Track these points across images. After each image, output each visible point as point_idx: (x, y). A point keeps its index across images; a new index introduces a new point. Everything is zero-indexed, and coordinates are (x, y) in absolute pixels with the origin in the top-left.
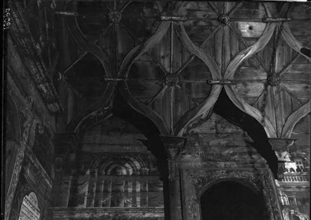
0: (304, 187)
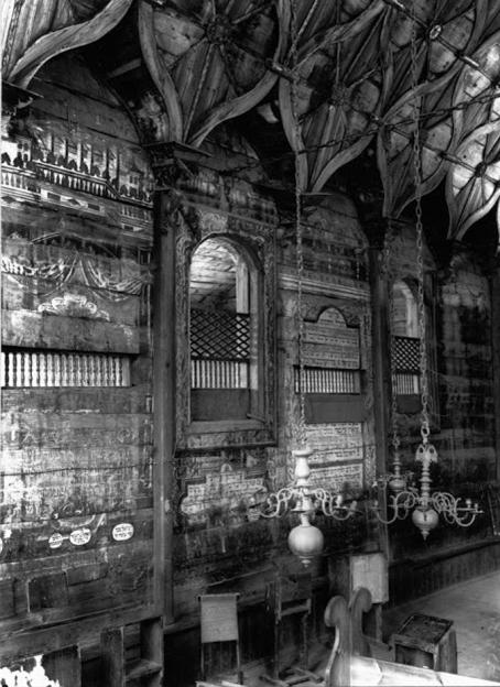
0: (19, 200)
